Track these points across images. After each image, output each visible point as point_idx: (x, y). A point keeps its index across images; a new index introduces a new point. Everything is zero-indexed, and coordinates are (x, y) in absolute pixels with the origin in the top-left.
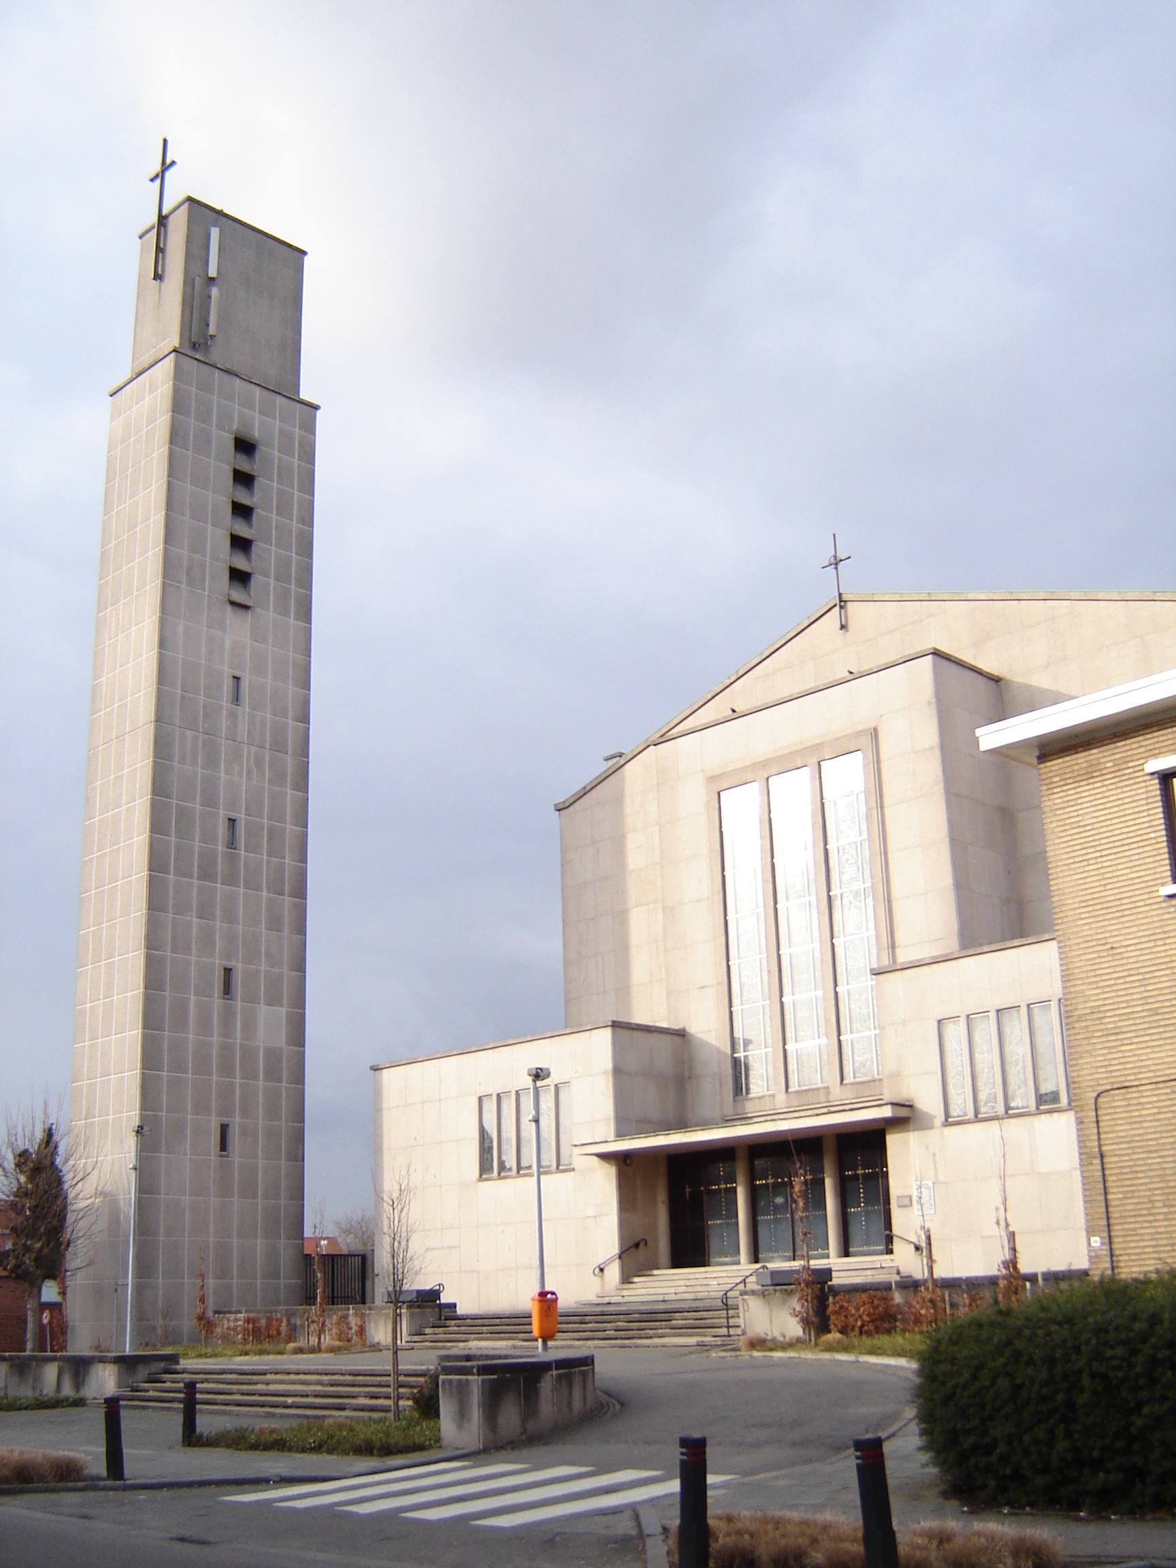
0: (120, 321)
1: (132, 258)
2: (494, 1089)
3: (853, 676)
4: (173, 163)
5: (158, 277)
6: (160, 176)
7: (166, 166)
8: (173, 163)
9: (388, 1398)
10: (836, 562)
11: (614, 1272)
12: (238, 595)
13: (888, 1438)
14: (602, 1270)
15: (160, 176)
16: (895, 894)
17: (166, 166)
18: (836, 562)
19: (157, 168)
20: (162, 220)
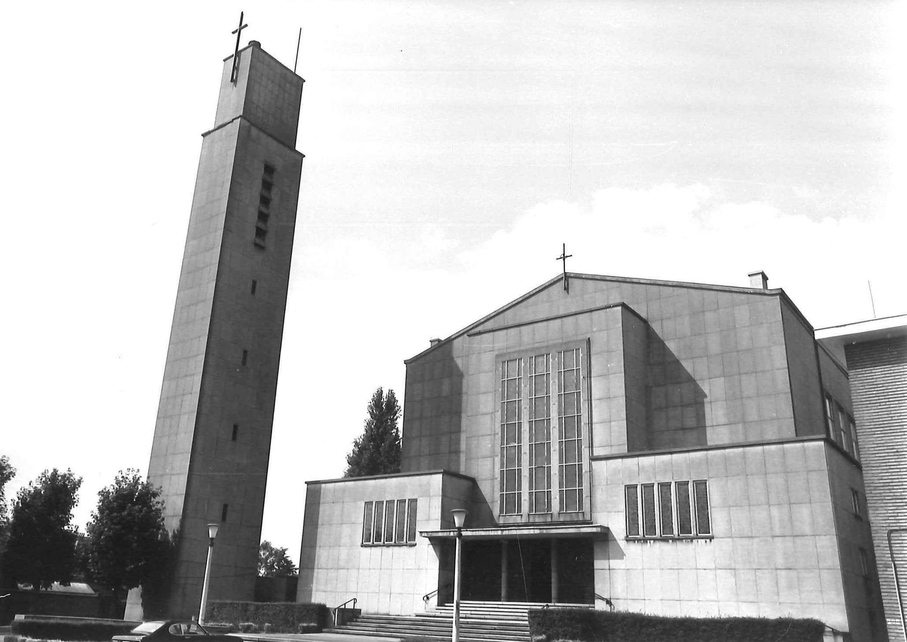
0: (201, 102)
1: (218, 71)
2: (375, 499)
3: (591, 311)
4: (246, 25)
5: (234, 80)
6: (238, 32)
7: (242, 26)
8: (246, 25)
9: (539, 381)
10: (564, 257)
11: (434, 600)
12: (258, 241)
13: (572, 498)
14: (428, 598)
15: (238, 32)
16: (704, 291)
17: (242, 26)
18: (564, 257)
19: (237, 27)
20: (238, 53)
